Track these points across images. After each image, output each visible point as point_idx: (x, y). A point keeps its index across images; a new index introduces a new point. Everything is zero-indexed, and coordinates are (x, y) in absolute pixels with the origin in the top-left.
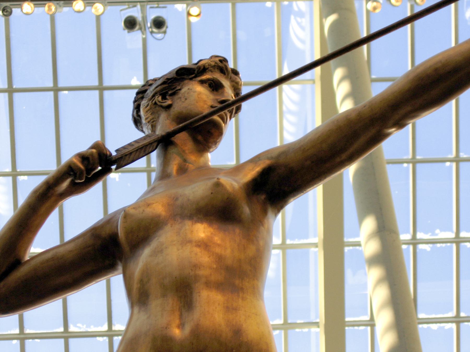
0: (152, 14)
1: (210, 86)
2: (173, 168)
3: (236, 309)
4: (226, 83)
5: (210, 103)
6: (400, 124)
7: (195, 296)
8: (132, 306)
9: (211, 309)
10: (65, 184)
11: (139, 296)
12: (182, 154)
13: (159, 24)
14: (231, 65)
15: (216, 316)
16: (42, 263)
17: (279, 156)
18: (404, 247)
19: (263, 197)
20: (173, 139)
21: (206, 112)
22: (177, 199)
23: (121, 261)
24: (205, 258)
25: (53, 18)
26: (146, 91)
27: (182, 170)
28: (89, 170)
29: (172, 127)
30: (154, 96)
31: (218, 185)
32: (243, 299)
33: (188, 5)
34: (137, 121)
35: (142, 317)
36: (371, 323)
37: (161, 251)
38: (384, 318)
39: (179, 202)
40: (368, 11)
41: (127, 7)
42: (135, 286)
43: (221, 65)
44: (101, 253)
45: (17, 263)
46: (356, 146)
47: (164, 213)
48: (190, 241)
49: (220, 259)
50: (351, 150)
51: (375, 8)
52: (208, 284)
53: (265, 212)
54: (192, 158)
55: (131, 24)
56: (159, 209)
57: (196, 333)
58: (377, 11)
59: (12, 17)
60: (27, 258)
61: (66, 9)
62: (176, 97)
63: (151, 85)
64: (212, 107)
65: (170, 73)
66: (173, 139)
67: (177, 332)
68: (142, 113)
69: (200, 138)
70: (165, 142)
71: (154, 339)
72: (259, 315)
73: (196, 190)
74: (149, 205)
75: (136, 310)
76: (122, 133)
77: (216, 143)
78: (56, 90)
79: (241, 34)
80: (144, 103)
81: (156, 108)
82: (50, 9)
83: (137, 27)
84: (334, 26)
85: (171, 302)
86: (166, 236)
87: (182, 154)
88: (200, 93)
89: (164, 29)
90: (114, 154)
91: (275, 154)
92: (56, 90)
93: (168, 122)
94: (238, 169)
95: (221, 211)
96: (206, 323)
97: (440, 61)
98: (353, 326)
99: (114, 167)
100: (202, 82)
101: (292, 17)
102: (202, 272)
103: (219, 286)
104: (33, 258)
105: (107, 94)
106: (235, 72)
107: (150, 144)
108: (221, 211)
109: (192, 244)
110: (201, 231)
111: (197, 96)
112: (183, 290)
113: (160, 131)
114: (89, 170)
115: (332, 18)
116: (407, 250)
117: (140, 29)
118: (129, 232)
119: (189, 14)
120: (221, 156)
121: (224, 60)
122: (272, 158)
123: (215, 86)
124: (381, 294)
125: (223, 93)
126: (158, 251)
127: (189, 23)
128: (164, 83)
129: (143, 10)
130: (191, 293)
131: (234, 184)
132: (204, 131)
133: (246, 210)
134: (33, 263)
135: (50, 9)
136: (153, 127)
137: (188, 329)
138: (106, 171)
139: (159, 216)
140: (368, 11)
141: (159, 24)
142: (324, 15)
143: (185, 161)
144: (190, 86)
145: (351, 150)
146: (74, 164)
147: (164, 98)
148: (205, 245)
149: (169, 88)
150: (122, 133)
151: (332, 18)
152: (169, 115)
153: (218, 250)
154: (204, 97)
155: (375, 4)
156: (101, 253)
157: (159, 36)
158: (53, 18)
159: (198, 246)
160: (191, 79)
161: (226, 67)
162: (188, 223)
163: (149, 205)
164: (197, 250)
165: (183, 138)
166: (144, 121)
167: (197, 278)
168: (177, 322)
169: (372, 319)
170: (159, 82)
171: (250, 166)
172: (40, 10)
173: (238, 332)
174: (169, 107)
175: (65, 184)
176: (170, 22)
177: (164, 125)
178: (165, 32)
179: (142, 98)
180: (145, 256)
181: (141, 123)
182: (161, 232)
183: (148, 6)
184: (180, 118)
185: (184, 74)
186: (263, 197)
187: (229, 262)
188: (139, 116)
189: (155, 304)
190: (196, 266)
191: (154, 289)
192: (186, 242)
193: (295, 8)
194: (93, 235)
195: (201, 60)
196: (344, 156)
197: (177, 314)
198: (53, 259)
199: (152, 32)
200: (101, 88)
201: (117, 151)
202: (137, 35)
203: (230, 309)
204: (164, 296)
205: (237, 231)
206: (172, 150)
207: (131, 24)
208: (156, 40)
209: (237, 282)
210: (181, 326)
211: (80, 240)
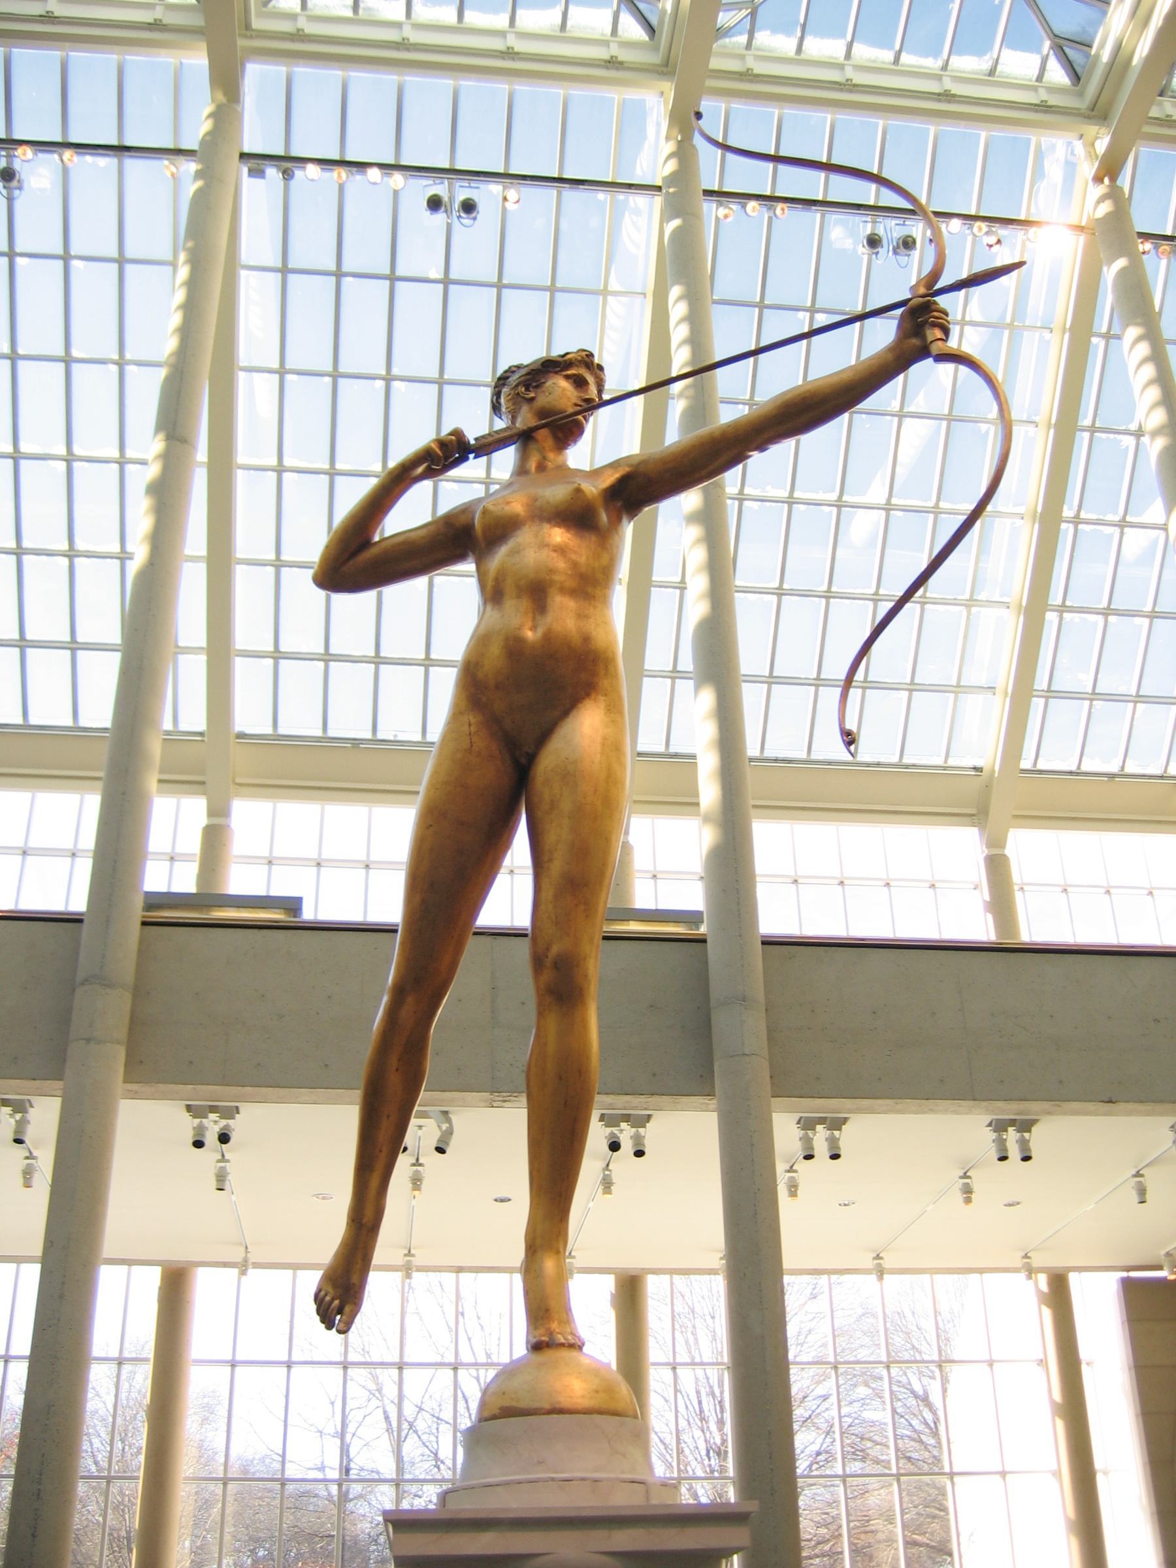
0: (462, 195)
1: (575, 382)
2: (532, 465)
3: (587, 617)
4: (591, 379)
5: (575, 400)
6: (762, 448)
7: (549, 600)
8: (485, 603)
9: (563, 614)
10: (420, 470)
11: (493, 593)
12: (542, 451)
13: (469, 207)
14: (596, 360)
15: (568, 621)
16: (393, 546)
17: (639, 464)
18: (729, 502)
19: (619, 504)
20: (534, 434)
21: (571, 410)
22: (536, 500)
23: (474, 553)
24: (561, 564)
25: (341, 188)
26: (508, 378)
27: (541, 468)
28: (446, 458)
29: (533, 423)
30: (517, 386)
31: (578, 490)
32: (595, 607)
33: (505, 188)
34: (496, 408)
35: (492, 614)
36: (682, 587)
37: (518, 552)
38: (699, 583)
39: (538, 504)
40: (717, 218)
41: (431, 182)
42: (490, 583)
43: (586, 359)
44: (452, 541)
45: (367, 543)
46: (716, 464)
47: (522, 513)
48: (547, 545)
49: (575, 565)
50: (711, 468)
51: (726, 217)
52: (562, 590)
53: (619, 520)
54: (551, 456)
55: (435, 204)
56: (517, 507)
57: (548, 638)
58: (729, 220)
59: (293, 183)
60: (377, 538)
61: (358, 177)
62: (539, 390)
63: (513, 372)
64: (576, 405)
65: (535, 362)
66: (534, 434)
67: (529, 635)
68: (502, 400)
69: (560, 435)
70: (525, 438)
71: (507, 639)
72: (607, 623)
73: (557, 493)
74: (508, 503)
75: (489, 608)
76: (474, 417)
77: (575, 441)
78: (339, 274)
79: (564, 226)
80: (505, 390)
81: (518, 400)
82: (339, 176)
83: (443, 209)
84: (677, 232)
85: (525, 603)
86: (525, 537)
87: (542, 451)
88: (564, 389)
89: (473, 215)
90: (472, 442)
91: (635, 462)
92: (339, 274)
93: (529, 415)
94: (596, 473)
95: (578, 516)
96: (557, 627)
97: (809, 391)
98: (661, 587)
99: (471, 456)
100: (567, 377)
101: (627, 214)
102: (556, 578)
103: (574, 593)
104: (383, 540)
105: (400, 285)
106: (600, 368)
107: (510, 437)
108: (578, 516)
109: (545, 547)
110: (558, 535)
111: (560, 391)
112: (537, 592)
113: (519, 425)
114: (446, 458)
115: (676, 222)
116: (732, 506)
117: (446, 211)
118: (487, 529)
119: (505, 199)
120: (580, 456)
121: (591, 355)
122: (632, 465)
123: (580, 383)
124: (698, 556)
125: (586, 391)
126: (515, 552)
127: (504, 210)
128: (528, 374)
129: (451, 189)
130: (546, 597)
131: (592, 489)
132: (566, 429)
133: (604, 517)
134: (384, 545)
135: (339, 176)
136: (514, 419)
137: (540, 632)
138: (463, 459)
139: (518, 515)
140: (717, 218)
141: (469, 207)
142: (665, 218)
143: (544, 458)
144: (554, 380)
145: (711, 468)
146: (432, 448)
147: (527, 389)
148: (561, 550)
149: (533, 380)
150: (474, 417)
151: (676, 222)
152: (531, 408)
153: (574, 557)
154: (569, 394)
155: (727, 211)
156: (452, 541)
157: (466, 222)
158: (341, 188)
159: (555, 551)
160: (556, 373)
161: (592, 362)
162: (546, 526)
163: (508, 503)
164: (554, 555)
165: (543, 433)
166: (503, 409)
167: (551, 583)
168: (530, 624)
169: (683, 581)
170: (523, 371)
171: (610, 472)
172: (327, 174)
173: (587, 639)
174: (532, 399)
175: (420, 470)
176: (481, 206)
177: (526, 419)
178: (475, 219)
179: (504, 385)
180: (500, 557)
181: (500, 410)
182: (518, 532)
183: (458, 184)
184: (543, 413)
185: (550, 366)
186: (619, 504)
187: (583, 570)
188: (500, 404)
189: (510, 604)
190: (552, 571)
191: (509, 587)
192: (544, 545)
193: (632, 204)
194: (446, 523)
195: (567, 354)
196: (703, 473)
197: (530, 615)
198: (404, 543)
199: (459, 217)
200: (393, 278)
201: (476, 439)
202: (440, 217)
203: (581, 616)
204: (518, 597)
205: (594, 538)
206: (532, 446)
207: (435, 204)
208: (464, 230)
209: (590, 590)
210: (534, 628)
211: (433, 528)
